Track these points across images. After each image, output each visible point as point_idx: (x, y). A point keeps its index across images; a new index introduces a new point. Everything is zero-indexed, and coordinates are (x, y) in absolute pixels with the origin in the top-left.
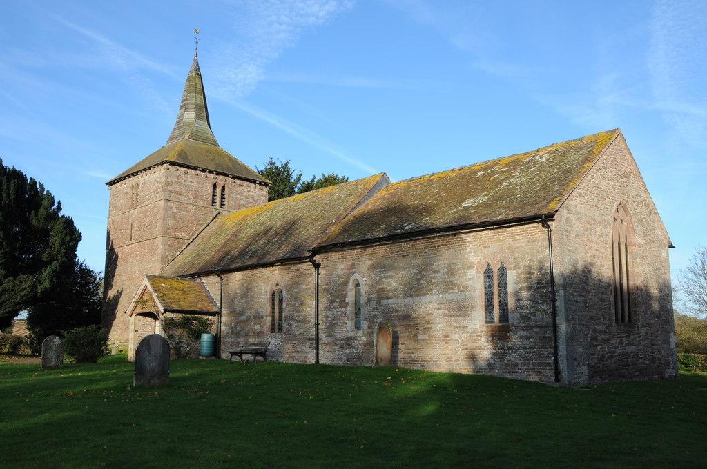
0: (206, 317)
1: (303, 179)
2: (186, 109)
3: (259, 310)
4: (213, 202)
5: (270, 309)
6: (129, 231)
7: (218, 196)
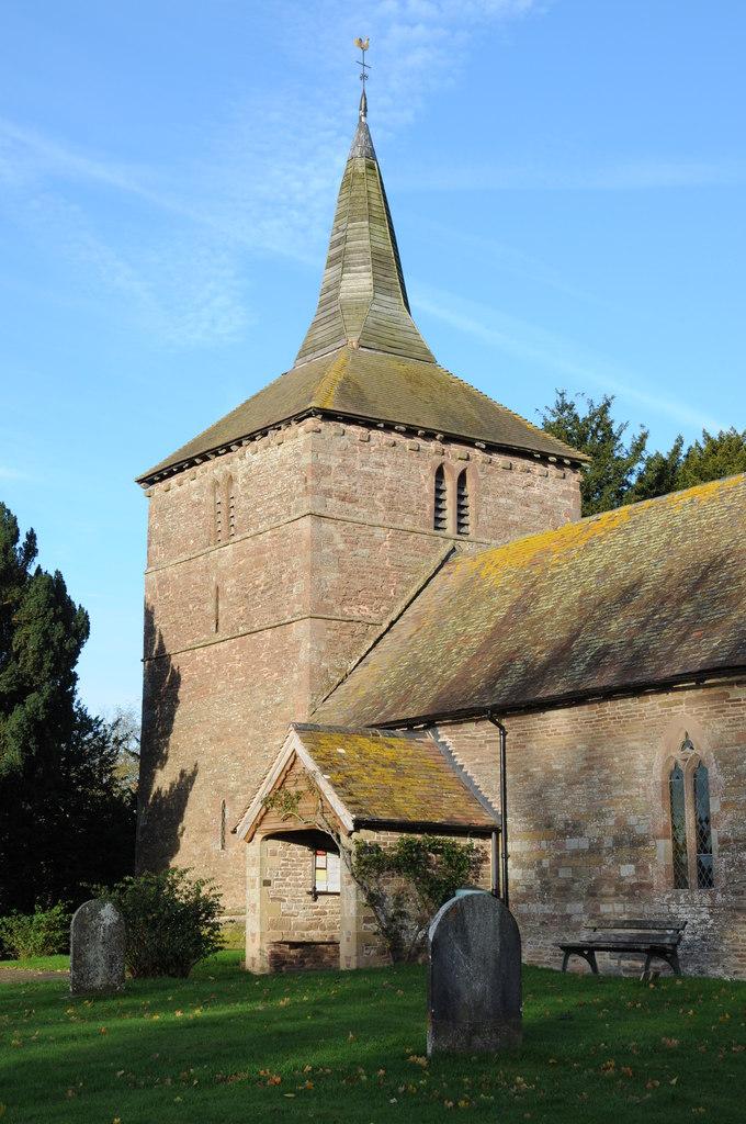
0: (464, 842)
1: (651, 449)
2: (345, 267)
3: (632, 820)
4: (437, 520)
5: (664, 819)
6: (209, 608)
7: (450, 503)
